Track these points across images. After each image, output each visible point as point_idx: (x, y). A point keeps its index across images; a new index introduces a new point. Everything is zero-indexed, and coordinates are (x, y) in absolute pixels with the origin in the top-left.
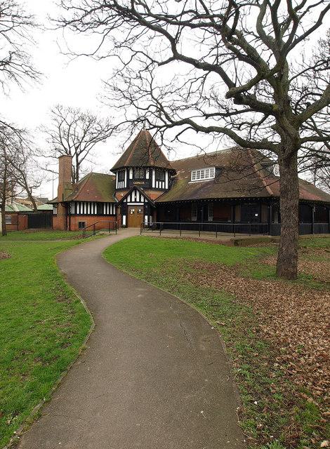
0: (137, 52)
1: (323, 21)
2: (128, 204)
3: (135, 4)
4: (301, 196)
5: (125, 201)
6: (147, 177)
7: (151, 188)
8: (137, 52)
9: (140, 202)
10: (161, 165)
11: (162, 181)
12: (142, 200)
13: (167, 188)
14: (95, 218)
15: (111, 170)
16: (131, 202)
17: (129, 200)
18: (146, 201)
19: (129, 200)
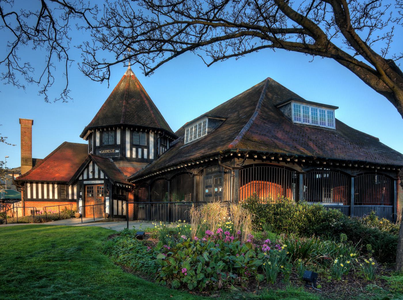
0: (8, 58)
1: (7, 14)
2: (85, 182)
3: (212, 11)
4: (33, 158)
5: (81, 178)
6: (119, 142)
7: (123, 158)
8: (8, 58)
9: (99, 179)
10: (158, 126)
11: (143, 147)
12: (102, 176)
13: (152, 157)
14: (57, 204)
15: (82, 136)
16: (88, 179)
17: (85, 177)
18: (106, 178)
19: (85, 177)
